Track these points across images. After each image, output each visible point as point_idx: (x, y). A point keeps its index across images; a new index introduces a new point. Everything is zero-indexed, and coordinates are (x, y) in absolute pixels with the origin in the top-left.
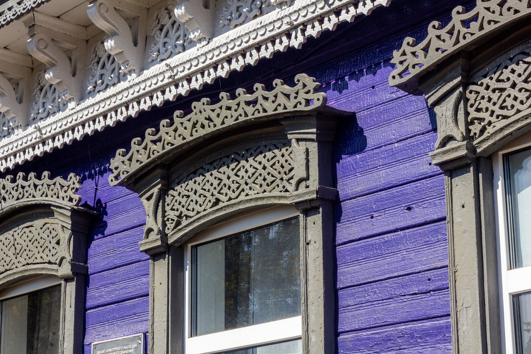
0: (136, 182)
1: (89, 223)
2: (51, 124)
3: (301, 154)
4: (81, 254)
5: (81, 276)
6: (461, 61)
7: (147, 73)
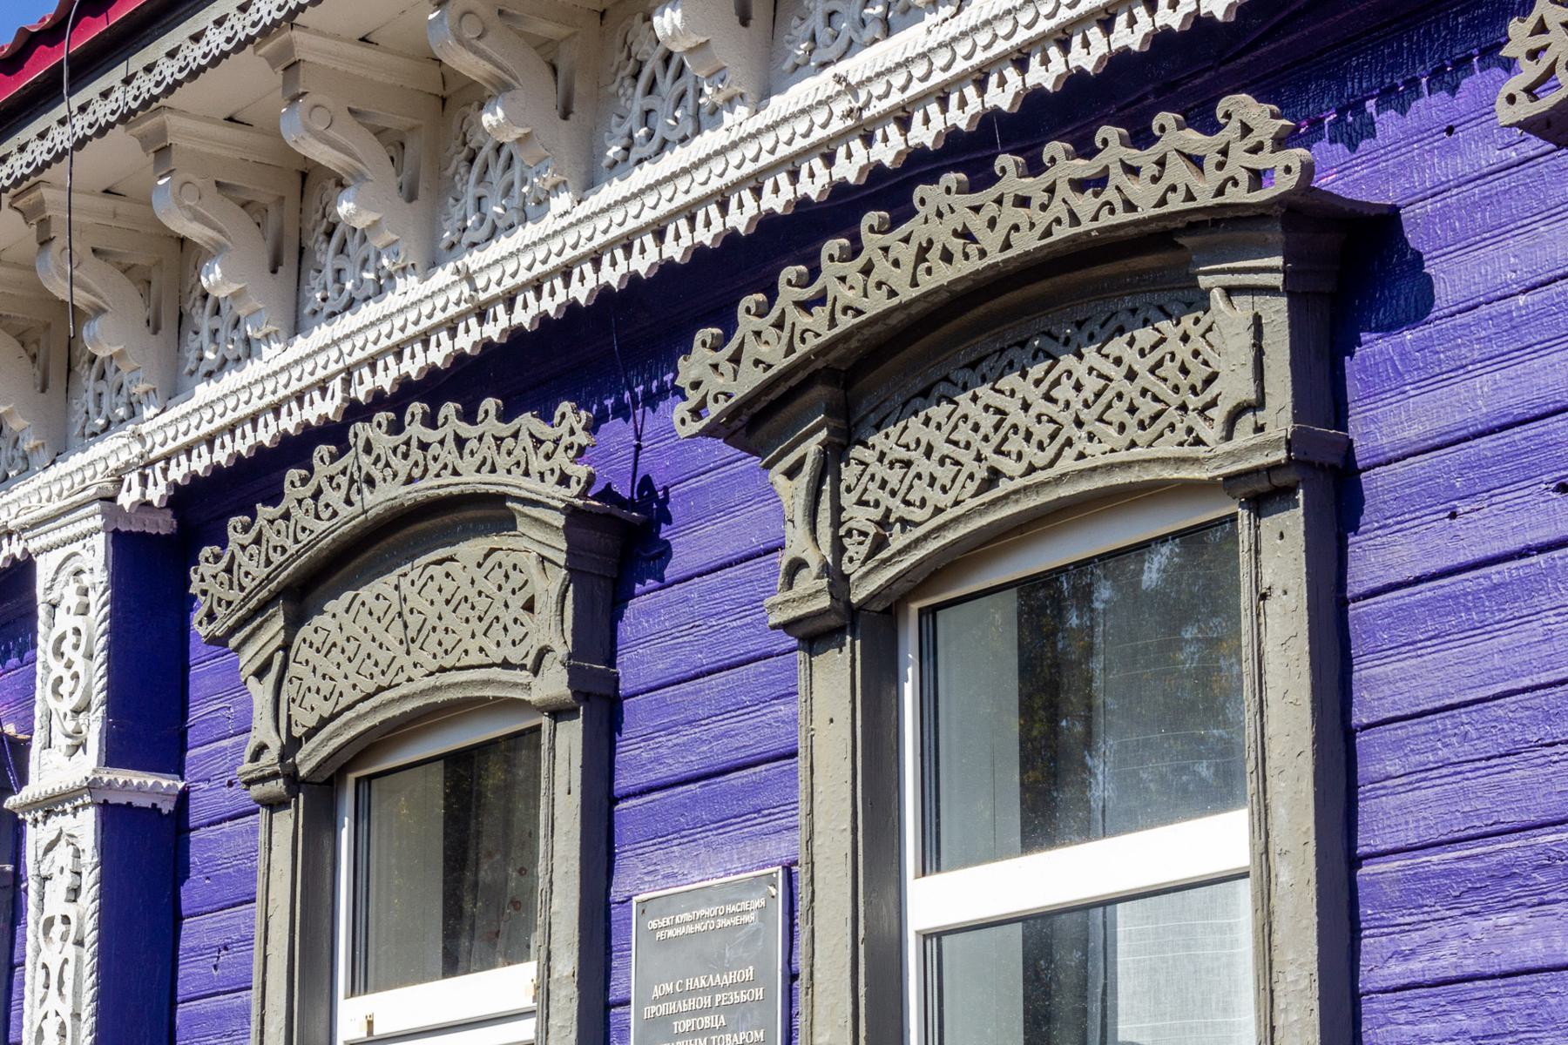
0: (755, 424)
1: (619, 546)
2: (502, 261)
3: (1239, 331)
4: (1324, 392)
5: (600, 704)
6: (819, 392)
7: (779, 105)
